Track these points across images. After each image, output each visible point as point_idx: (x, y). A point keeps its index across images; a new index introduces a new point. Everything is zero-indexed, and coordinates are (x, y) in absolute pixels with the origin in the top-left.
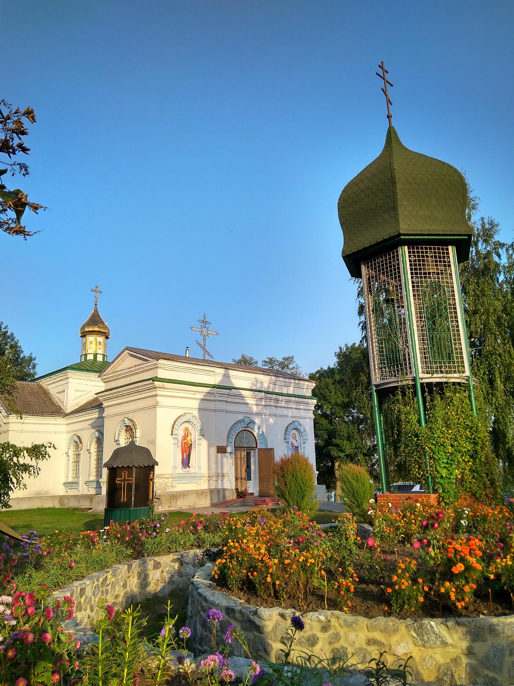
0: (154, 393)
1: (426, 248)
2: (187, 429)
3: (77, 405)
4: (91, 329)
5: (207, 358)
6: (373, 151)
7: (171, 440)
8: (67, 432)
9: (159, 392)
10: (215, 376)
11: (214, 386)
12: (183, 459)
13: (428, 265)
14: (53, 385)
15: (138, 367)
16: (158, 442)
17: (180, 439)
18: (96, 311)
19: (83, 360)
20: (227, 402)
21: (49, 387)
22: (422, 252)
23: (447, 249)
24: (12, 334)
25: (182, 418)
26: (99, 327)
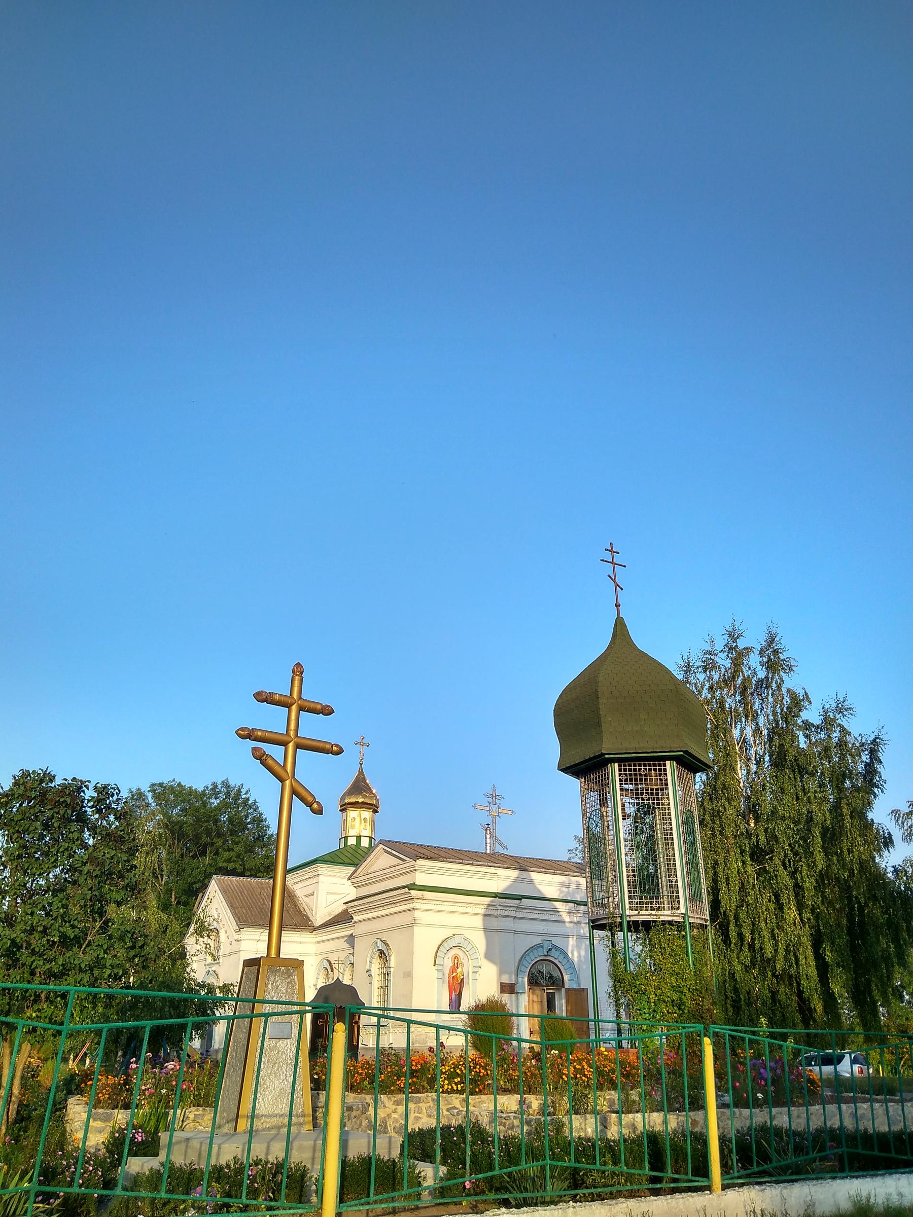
0: (410, 906)
1: (639, 765)
2: (456, 957)
3: (330, 914)
4: (353, 800)
5: (499, 849)
6: (597, 644)
7: (433, 972)
8: (317, 955)
9: (416, 905)
10: (501, 879)
11: (496, 895)
12: (450, 999)
13: (651, 780)
14: (301, 885)
15: (393, 869)
16: (415, 974)
17: (447, 972)
18: (361, 773)
19: (342, 846)
20: (515, 918)
21: (296, 887)
22: (635, 770)
23: (665, 765)
24: (255, 802)
25: (449, 941)
26: (364, 797)
